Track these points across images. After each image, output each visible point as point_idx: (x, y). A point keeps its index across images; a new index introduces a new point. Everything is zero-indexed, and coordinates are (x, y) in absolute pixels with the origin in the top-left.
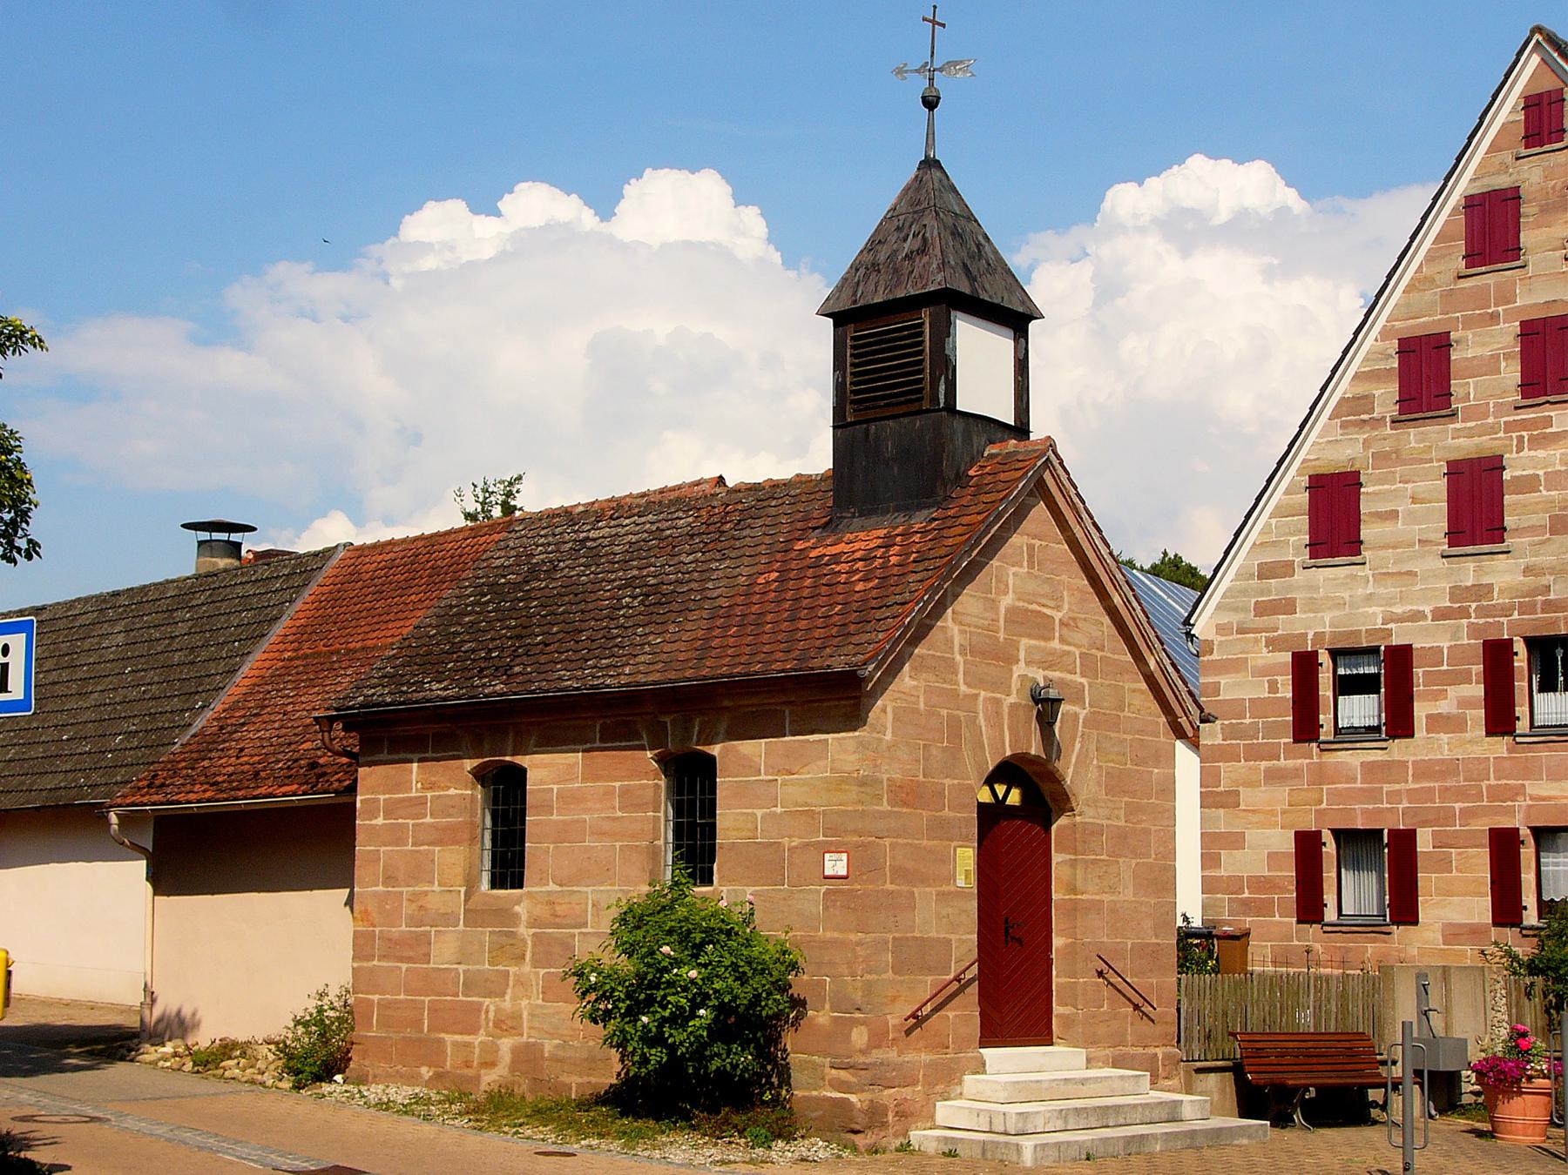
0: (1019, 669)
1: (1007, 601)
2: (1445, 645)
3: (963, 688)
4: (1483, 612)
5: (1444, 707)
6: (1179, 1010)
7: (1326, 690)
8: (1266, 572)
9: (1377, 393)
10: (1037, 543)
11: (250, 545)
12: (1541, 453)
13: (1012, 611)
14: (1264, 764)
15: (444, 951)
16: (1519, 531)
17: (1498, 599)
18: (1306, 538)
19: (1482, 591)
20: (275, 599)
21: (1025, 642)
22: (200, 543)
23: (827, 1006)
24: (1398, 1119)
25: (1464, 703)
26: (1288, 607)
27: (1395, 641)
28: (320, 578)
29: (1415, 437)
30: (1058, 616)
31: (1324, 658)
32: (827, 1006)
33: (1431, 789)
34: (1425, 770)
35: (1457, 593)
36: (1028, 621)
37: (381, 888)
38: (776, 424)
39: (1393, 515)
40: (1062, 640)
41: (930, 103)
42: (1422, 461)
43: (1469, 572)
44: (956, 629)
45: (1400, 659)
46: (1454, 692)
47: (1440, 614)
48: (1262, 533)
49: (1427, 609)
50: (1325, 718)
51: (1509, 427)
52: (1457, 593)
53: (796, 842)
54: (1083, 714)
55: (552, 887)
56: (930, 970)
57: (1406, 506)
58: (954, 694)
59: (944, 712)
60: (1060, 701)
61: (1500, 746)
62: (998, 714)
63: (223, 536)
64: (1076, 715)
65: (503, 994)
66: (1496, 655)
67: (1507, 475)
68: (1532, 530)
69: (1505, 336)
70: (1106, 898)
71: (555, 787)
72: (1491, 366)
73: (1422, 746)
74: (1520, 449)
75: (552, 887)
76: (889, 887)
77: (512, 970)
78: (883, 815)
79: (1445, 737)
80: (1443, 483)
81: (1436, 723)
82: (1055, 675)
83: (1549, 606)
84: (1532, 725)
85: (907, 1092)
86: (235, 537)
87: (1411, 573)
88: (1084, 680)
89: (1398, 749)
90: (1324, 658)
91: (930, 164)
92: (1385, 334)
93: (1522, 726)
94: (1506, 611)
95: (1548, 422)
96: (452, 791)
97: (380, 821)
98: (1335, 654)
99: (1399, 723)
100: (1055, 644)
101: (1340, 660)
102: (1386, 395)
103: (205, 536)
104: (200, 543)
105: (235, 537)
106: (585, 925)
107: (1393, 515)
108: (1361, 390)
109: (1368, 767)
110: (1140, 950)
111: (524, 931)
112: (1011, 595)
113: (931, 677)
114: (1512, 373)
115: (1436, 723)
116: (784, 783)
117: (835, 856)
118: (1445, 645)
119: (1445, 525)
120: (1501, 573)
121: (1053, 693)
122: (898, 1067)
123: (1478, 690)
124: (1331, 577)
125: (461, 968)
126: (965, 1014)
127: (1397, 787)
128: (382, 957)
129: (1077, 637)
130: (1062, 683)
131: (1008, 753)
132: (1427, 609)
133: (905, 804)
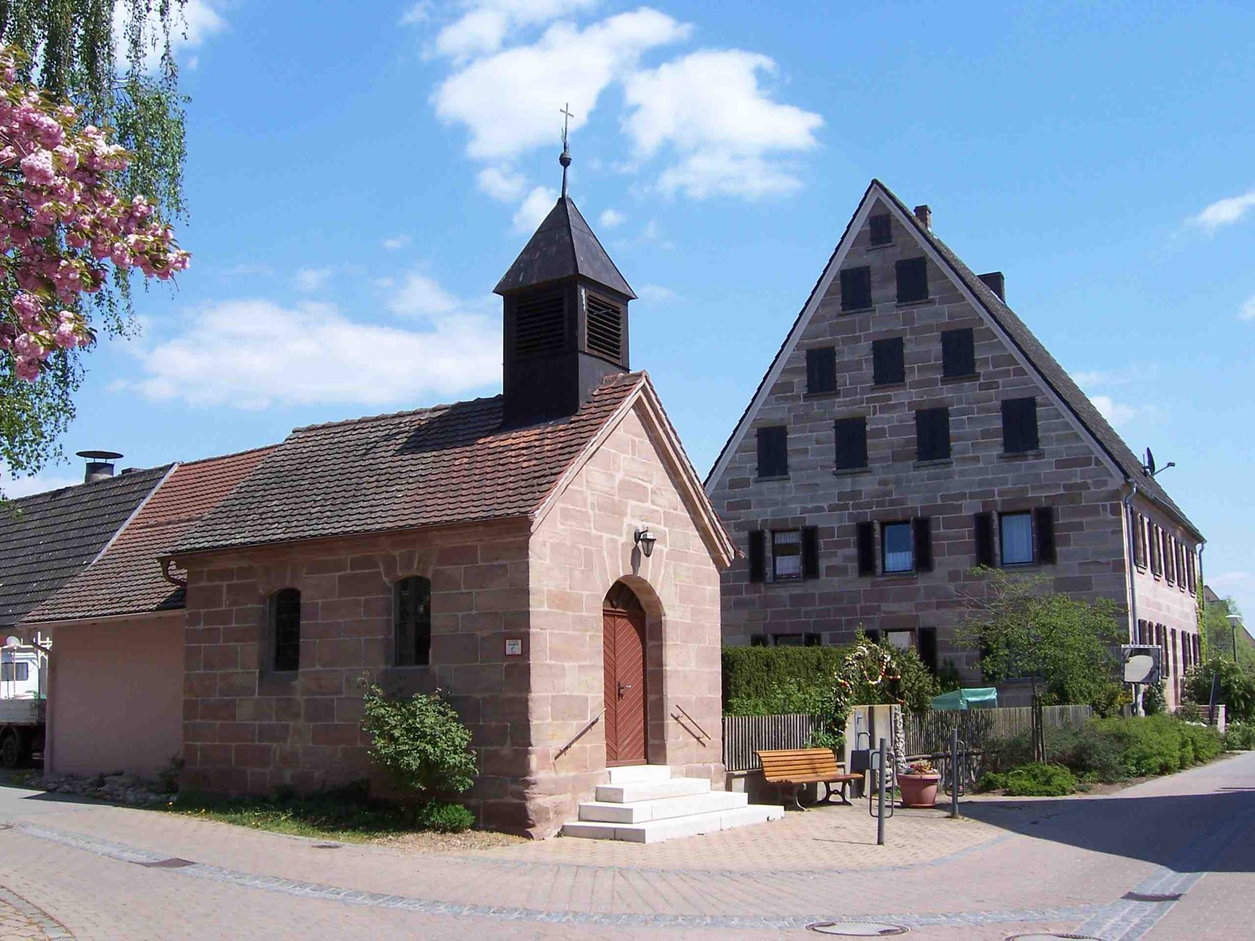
0: (627, 520)
1: (619, 476)
2: (835, 526)
3: (594, 532)
4: (855, 506)
5: (836, 561)
6: (723, 739)
7: (768, 554)
8: (734, 484)
9: (796, 381)
10: (637, 439)
11: (119, 467)
12: (886, 416)
13: (622, 482)
14: (733, 597)
15: (245, 710)
16: (875, 460)
17: (864, 499)
18: (756, 465)
19: (855, 494)
20: (135, 496)
21: (631, 502)
22: (89, 465)
23: (509, 742)
24: (831, 799)
25: (847, 559)
26: (747, 505)
27: (808, 524)
28: (162, 483)
29: (816, 407)
30: (649, 486)
31: (768, 535)
32: (509, 742)
33: (829, 610)
34: (825, 598)
35: (841, 496)
36: (631, 489)
37: (202, 671)
38: (469, 361)
39: (805, 451)
40: (653, 502)
41: (565, 162)
42: (821, 420)
43: (848, 484)
44: (589, 492)
45: (810, 536)
46: (840, 552)
47: (832, 508)
48: (731, 461)
49: (825, 505)
50: (769, 570)
51: (869, 400)
52: (841, 496)
53: (486, 633)
54: (666, 550)
55: (318, 667)
56: (575, 717)
57: (812, 445)
58: (587, 534)
59: (582, 547)
60: (653, 540)
61: (865, 584)
62: (616, 549)
63: (103, 461)
64: (662, 551)
65: (285, 740)
66: (864, 531)
67: (868, 428)
68: (881, 459)
69: (864, 349)
70: (680, 668)
71: (320, 601)
72: (857, 365)
73: (826, 584)
74: (875, 413)
75: (318, 667)
76: (548, 661)
77: (291, 723)
78: (547, 614)
79: (836, 579)
80: (832, 433)
81: (832, 571)
82: (649, 525)
83: (892, 503)
84: (884, 571)
85: (562, 797)
86: (110, 461)
87: (817, 485)
88: (667, 530)
89: (811, 587)
90: (768, 535)
91: (562, 201)
92: (798, 347)
93: (879, 570)
94: (869, 505)
95: (889, 398)
96: (249, 606)
97: (201, 626)
98: (773, 532)
99: (810, 569)
100: (648, 505)
101: (777, 535)
102: (800, 381)
103: (91, 460)
104: (89, 465)
105: (110, 461)
106: (341, 692)
107: (805, 451)
108: (787, 378)
109: (792, 597)
110: (700, 700)
111: (299, 697)
112: (622, 472)
113: (574, 523)
114: (869, 371)
115: (832, 571)
116: (478, 594)
117: (512, 642)
118: (835, 526)
119: (834, 457)
120: (867, 484)
121: (650, 536)
122: (556, 782)
123: (853, 551)
124: (770, 488)
125: (257, 723)
126: (597, 743)
127: (810, 608)
128: (202, 717)
129: (661, 501)
130: (654, 531)
131: (622, 575)
132: (825, 505)
133: (558, 607)
